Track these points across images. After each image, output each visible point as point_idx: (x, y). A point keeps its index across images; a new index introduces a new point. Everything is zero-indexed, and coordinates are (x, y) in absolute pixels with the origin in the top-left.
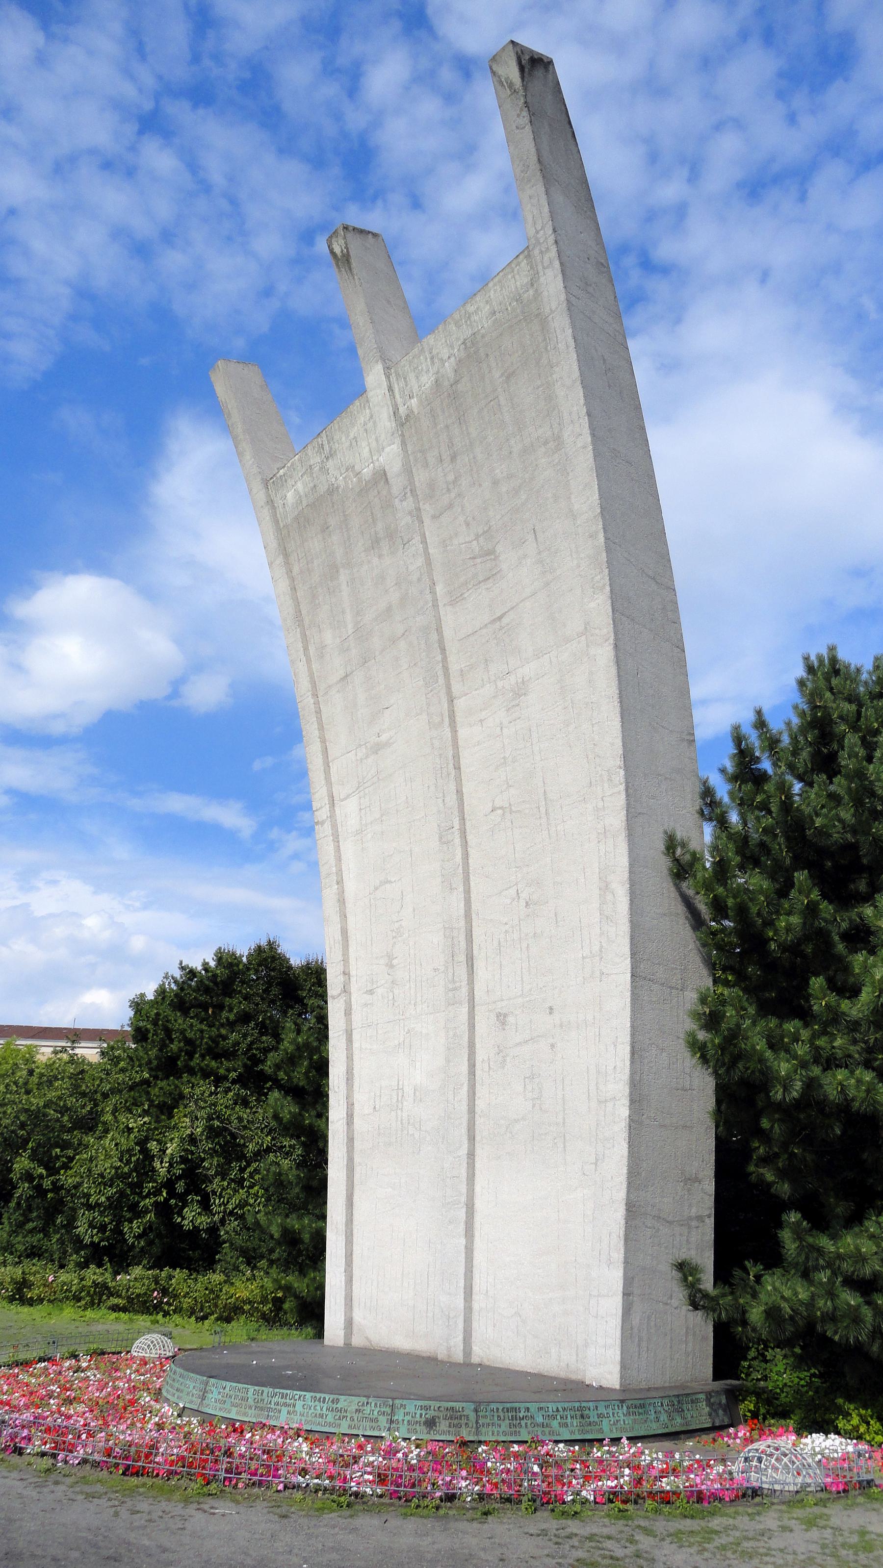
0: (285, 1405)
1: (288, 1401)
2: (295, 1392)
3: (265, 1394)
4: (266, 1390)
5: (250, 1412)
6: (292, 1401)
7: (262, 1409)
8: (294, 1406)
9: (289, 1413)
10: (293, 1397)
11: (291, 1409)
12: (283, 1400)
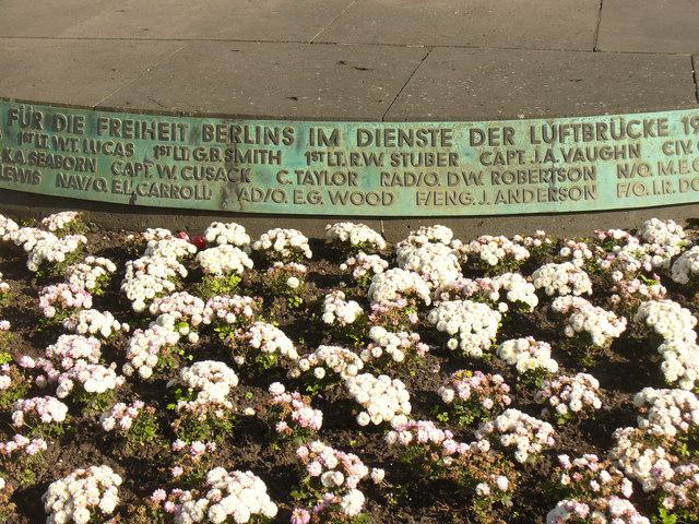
0: (601, 154)
1: (611, 143)
2: (628, 118)
3: (521, 139)
4: (521, 127)
5: (476, 192)
6: (626, 141)
7: (519, 177)
8: (635, 151)
9: (622, 172)
10: (626, 130)
11: (630, 161)
12: (595, 144)
